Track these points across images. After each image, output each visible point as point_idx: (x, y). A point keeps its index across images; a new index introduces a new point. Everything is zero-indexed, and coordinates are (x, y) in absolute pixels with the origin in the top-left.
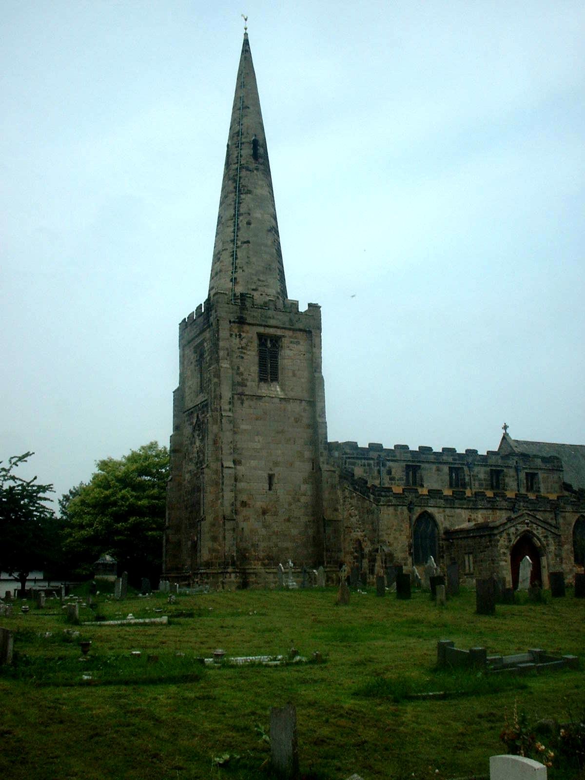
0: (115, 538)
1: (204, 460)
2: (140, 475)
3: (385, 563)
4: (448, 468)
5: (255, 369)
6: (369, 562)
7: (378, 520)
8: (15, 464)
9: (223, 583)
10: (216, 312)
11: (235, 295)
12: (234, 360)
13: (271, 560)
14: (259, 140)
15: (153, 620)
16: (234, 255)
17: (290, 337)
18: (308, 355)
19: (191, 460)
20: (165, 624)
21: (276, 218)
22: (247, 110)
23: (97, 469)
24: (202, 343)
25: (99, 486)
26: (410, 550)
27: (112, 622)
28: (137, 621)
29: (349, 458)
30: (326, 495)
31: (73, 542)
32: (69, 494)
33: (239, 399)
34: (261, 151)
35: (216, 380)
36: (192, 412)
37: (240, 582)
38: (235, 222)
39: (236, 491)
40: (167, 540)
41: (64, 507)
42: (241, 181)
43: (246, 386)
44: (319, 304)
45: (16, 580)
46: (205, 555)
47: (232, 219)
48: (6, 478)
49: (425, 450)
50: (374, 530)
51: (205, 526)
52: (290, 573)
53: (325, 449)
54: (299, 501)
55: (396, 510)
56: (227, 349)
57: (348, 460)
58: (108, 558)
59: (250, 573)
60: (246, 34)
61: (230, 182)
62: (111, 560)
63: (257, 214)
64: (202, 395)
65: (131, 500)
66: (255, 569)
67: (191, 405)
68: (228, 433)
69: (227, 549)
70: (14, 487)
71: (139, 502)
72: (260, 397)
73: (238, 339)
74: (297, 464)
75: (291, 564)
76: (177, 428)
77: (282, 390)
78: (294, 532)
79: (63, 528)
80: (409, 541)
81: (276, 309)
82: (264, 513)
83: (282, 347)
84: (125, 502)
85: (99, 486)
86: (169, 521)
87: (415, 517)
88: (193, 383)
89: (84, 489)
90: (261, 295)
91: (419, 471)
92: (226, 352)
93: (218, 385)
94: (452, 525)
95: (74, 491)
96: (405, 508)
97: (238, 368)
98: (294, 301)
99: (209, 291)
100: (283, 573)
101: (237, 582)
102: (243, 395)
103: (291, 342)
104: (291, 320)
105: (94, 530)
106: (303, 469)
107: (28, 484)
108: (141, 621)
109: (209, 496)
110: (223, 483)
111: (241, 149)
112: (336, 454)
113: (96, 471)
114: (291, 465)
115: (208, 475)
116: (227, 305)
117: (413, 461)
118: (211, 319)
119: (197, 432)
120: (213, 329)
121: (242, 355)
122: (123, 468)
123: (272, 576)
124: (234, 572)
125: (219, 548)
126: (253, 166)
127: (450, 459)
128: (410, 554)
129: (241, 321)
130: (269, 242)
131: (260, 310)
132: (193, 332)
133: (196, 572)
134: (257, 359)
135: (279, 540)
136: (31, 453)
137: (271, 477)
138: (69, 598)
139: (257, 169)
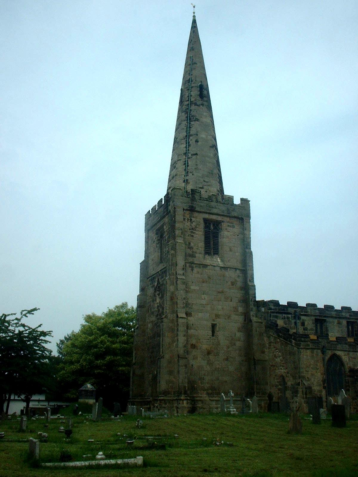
0: (95, 371)
1: (163, 312)
2: (114, 327)
3: (306, 394)
4: (346, 321)
5: (202, 244)
6: (292, 393)
7: (299, 360)
8: (25, 315)
9: (177, 408)
10: (173, 202)
11: (187, 192)
12: (187, 237)
13: (214, 391)
14: (204, 85)
15: (126, 460)
16: (186, 164)
17: (229, 222)
18: (241, 236)
19: (153, 313)
20: (140, 466)
21: (216, 138)
22: (195, 65)
23: (84, 321)
24: (162, 227)
25: (84, 333)
26: (324, 384)
27: (78, 464)
28: (107, 462)
29: (273, 312)
30: (256, 340)
31: (65, 373)
32: (64, 339)
33: (190, 266)
34: (205, 92)
35: (173, 252)
36: (154, 278)
37: (190, 408)
38: (186, 141)
39: (188, 336)
40: (134, 373)
41: (60, 348)
42: (191, 112)
43: (195, 257)
44: (249, 199)
45: (23, 400)
46: (163, 385)
47: (185, 139)
48: (18, 325)
49: (329, 308)
50: (296, 368)
51: (164, 363)
52: (231, 402)
53: (254, 306)
54: (235, 344)
55: (312, 352)
56: (181, 229)
57: (272, 314)
58: (89, 386)
59: (197, 400)
60: (194, 16)
61: (183, 114)
62: (91, 387)
63: (203, 135)
64: (161, 265)
65: (108, 343)
66: (201, 397)
67: (154, 272)
68: (181, 291)
69: (180, 381)
70: (23, 331)
71: (114, 346)
72: (205, 266)
73: (189, 223)
74: (234, 317)
75: (232, 394)
76: (142, 289)
77: (222, 261)
78: (231, 369)
79: (58, 363)
80: (323, 377)
81: (217, 202)
82: (209, 353)
83: (221, 229)
84: (103, 345)
85: (84, 333)
86: (135, 359)
87: (327, 358)
88: (156, 256)
89: (74, 336)
90: (206, 192)
91: (325, 324)
92: (181, 231)
93: (174, 256)
94: (355, 365)
95: (68, 337)
96: (319, 351)
97: (190, 243)
98: (231, 196)
99: (167, 190)
100: (225, 401)
101: (188, 407)
102: (193, 263)
103: (228, 226)
104: (228, 210)
105: (80, 365)
106: (238, 320)
107: (34, 330)
108: (113, 462)
109: (167, 339)
110: (178, 330)
111: (191, 91)
112: (263, 309)
113: (84, 323)
114: (229, 317)
115: (166, 324)
116: (181, 197)
117: (320, 316)
118: (170, 208)
119: (158, 292)
120: (171, 215)
121: (192, 234)
122: (102, 321)
123: (214, 403)
124: (185, 400)
125: (175, 380)
126: (199, 103)
127: (347, 315)
128: (324, 387)
129: (192, 210)
130: (212, 155)
131: (205, 201)
132: (156, 219)
133: (156, 398)
134: (203, 238)
135: (219, 375)
136: (37, 308)
137: (213, 326)
138: (56, 417)
139: (202, 105)
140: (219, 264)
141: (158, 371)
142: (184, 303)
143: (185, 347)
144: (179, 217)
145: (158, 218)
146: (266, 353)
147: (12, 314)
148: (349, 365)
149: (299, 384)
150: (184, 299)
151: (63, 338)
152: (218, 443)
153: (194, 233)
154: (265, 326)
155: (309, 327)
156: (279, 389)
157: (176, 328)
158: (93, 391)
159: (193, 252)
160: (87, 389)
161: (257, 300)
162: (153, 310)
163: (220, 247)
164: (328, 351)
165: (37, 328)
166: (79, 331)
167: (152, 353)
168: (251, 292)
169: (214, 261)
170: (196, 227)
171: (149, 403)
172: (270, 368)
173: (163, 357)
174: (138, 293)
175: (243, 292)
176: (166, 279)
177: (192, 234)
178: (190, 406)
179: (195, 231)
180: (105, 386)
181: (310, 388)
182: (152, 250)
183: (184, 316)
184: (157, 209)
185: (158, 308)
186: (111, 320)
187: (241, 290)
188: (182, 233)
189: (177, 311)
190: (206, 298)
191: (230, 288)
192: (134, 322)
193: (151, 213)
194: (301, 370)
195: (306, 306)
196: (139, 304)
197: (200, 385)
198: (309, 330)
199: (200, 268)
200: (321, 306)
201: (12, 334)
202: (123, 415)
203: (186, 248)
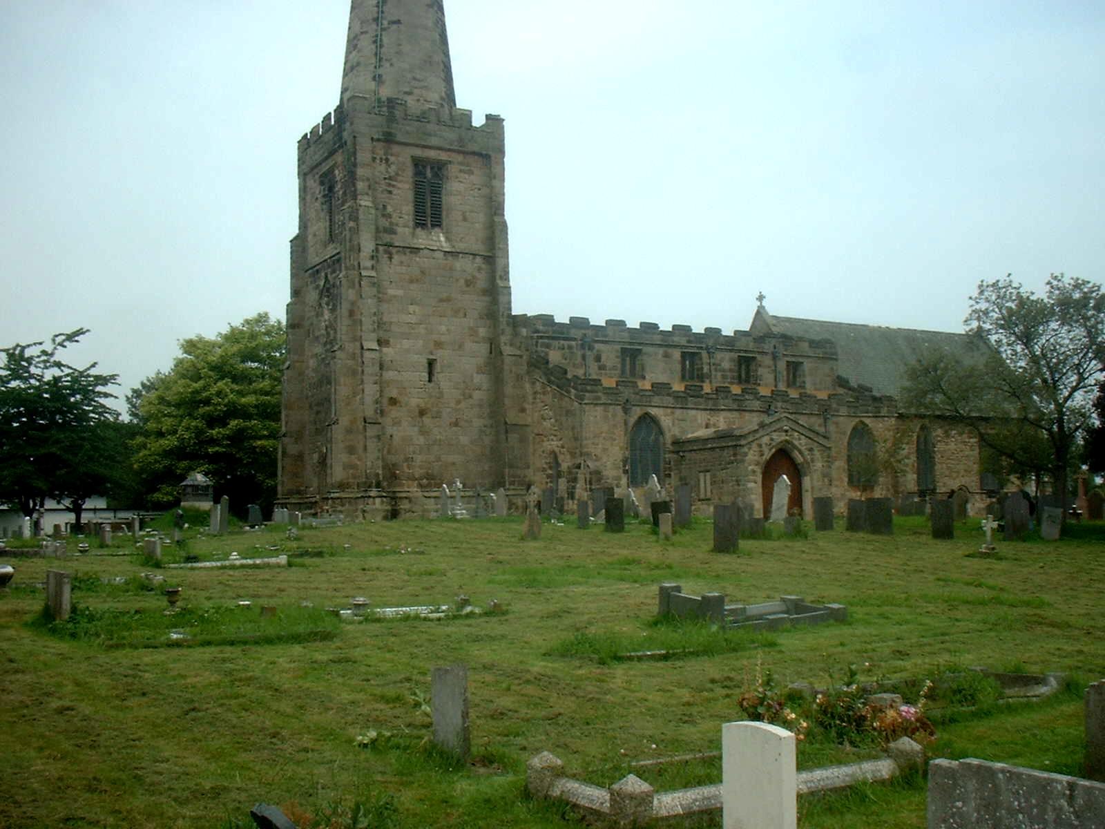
1: (335, 339)
2: (243, 362)
5: (408, 209)
6: (568, 482)
8: (61, 345)
10: (352, 124)
13: (431, 481)
16: (377, 42)
17: (461, 164)
19: (317, 338)
23: (181, 351)
24: (331, 171)
25: (184, 376)
26: (624, 466)
27: (208, 564)
29: (541, 337)
30: (509, 390)
31: (149, 455)
32: (141, 388)
35: (352, 224)
36: (317, 271)
39: (382, 384)
40: (284, 453)
44: (502, 117)
45: (68, 509)
46: (338, 473)
51: (338, 432)
54: (470, 397)
56: (368, 179)
59: (401, 498)
64: (331, 246)
67: (317, 260)
72: (415, 250)
73: (384, 165)
74: (469, 345)
75: (459, 485)
76: (296, 292)
81: (439, 122)
82: (422, 413)
84: (223, 399)
85: (184, 376)
88: (320, 227)
91: (639, 357)
93: (356, 231)
97: (384, 206)
103: (461, 171)
109: (342, 390)
110: (363, 371)
112: (524, 331)
113: (180, 354)
115: (342, 360)
118: (345, 134)
122: (219, 351)
125: (358, 463)
127: (683, 342)
128: (626, 472)
129: (389, 139)
130: (430, 24)
134: (410, 196)
137: (431, 364)
140: (442, 247)
141: (329, 446)
142: (374, 322)
143: (377, 403)
144: (363, 156)
145: (324, 153)
146: (528, 412)
147: (35, 344)
148: (672, 433)
149: (579, 467)
150: (375, 314)
151: (138, 386)
152: (403, 552)
153: (393, 186)
154: (528, 364)
155: (609, 364)
156: (549, 476)
157: (360, 369)
158: (208, 486)
159: (391, 223)
160: (196, 483)
161: (513, 314)
162: (317, 334)
163: (444, 213)
164: (634, 408)
165: (88, 369)
166: (169, 370)
167: (318, 413)
168: (502, 299)
169: (432, 240)
170: (397, 174)
171: (313, 505)
172: (534, 438)
173: (336, 422)
174: (289, 300)
175: (487, 299)
176: (341, 276)
177: (389, 189)
178: (389, 508)
179: (395, 183)
180: (229, 477)
181: (598, 473)
182: (312, 214)
183: (375, 346)
184: (320, 133)
185: (326, 330)
186: (235, 348)
187: (484, 295)
188: (369, 187)
189: (361, 337)
190: (417, 310)
191: (463, 293)
192: (284, 351)
193: (309, 137)
194: (585, 442)
195: (606, 323)
196: (290, 322)
197: (407, 470)
198: (610, 370)
199: (405, 254)
200: (633, 323)
201: (38, 384)
202: (266, 525)
203: (377, 216)
